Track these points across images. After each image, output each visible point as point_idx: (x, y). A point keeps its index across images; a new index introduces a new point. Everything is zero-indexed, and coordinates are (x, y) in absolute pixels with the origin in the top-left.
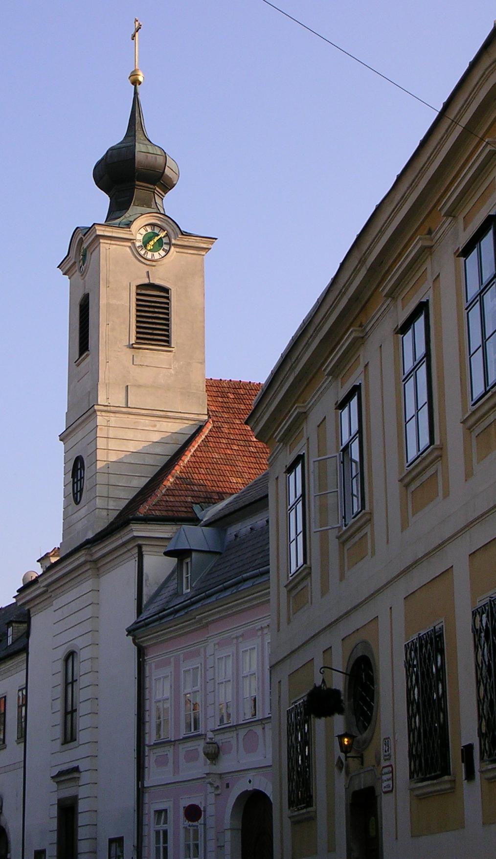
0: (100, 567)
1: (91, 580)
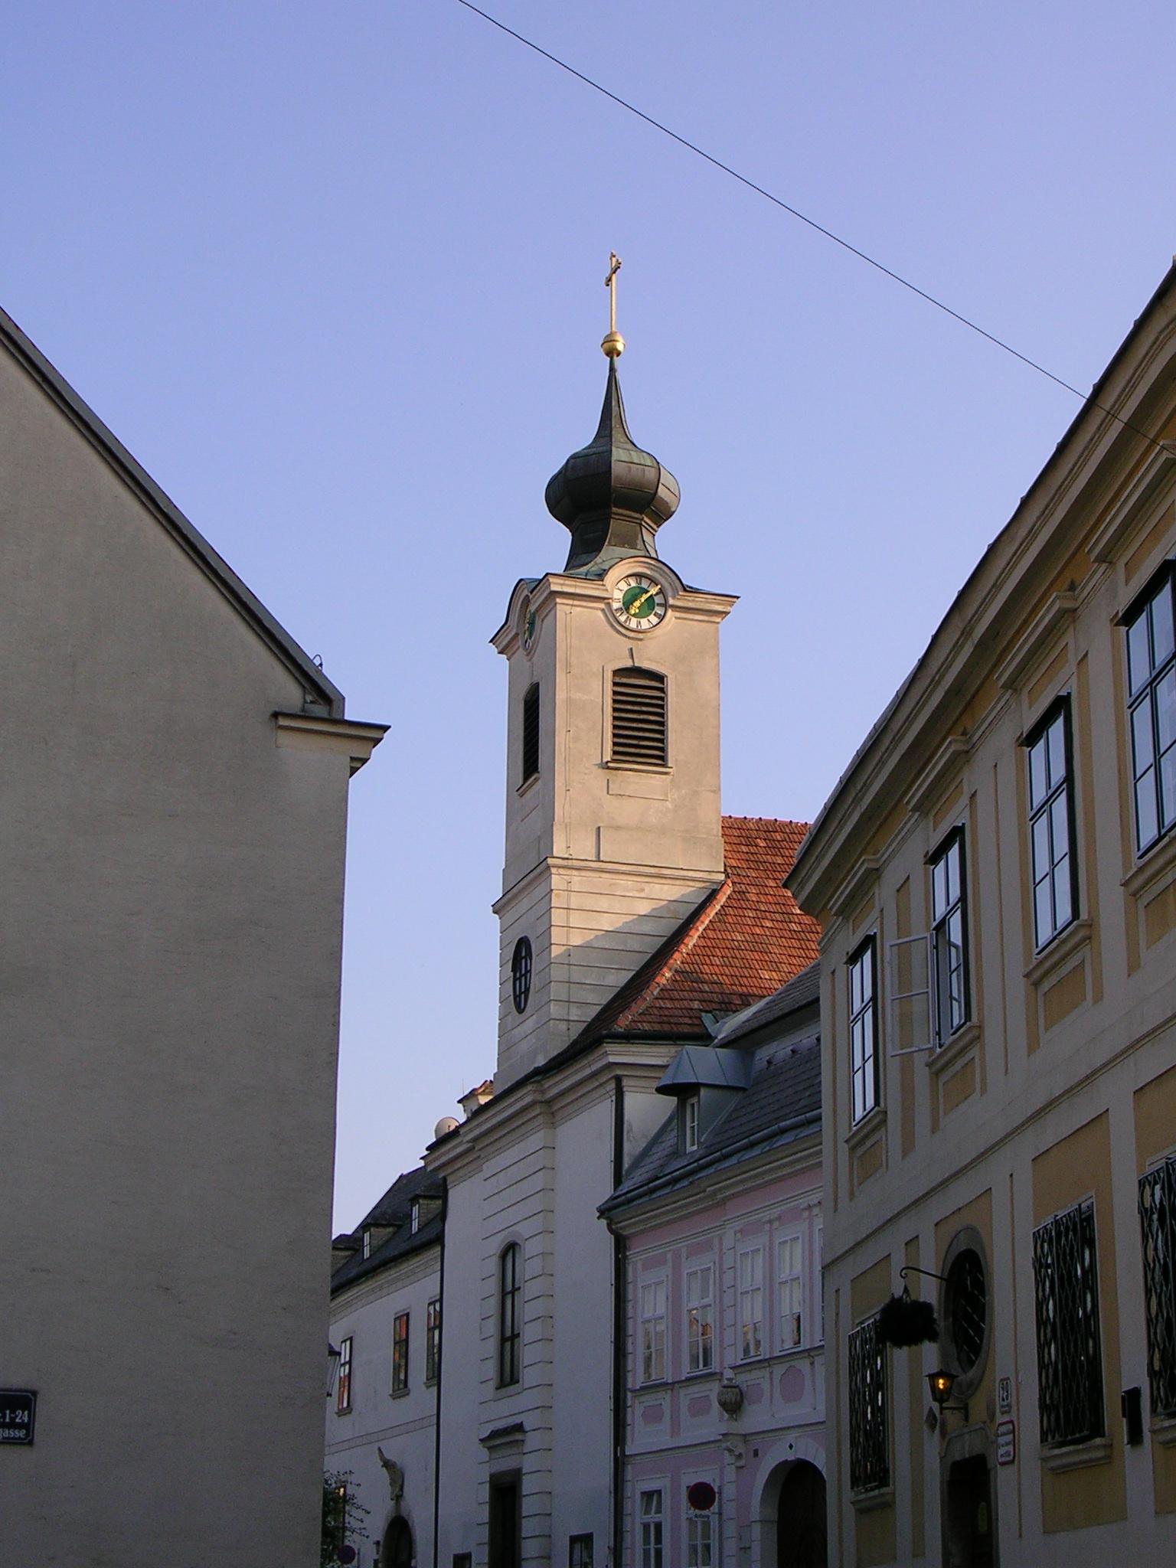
0: (556, 1111)
1: (542, 1131)
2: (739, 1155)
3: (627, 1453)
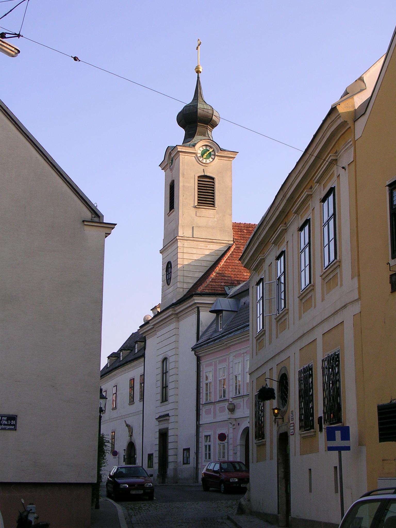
0: (179, 317)
1: (175, 323)
2: (234, 333)
3: (200, 424)
